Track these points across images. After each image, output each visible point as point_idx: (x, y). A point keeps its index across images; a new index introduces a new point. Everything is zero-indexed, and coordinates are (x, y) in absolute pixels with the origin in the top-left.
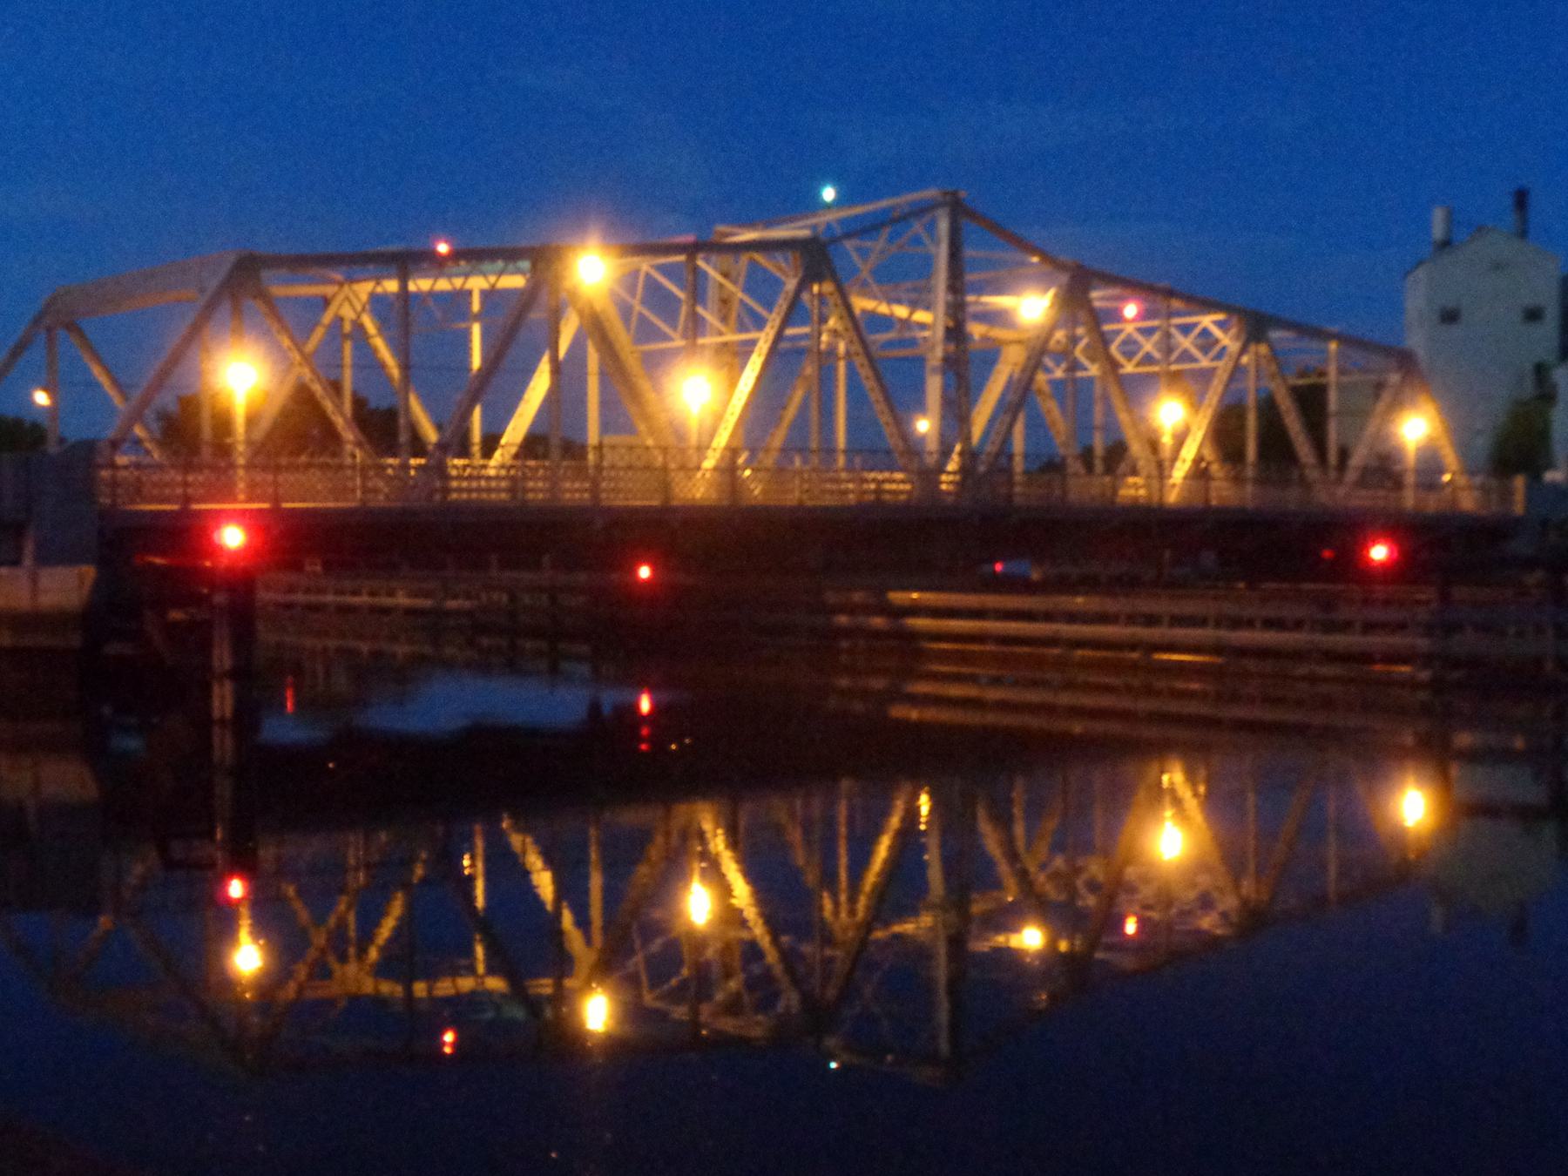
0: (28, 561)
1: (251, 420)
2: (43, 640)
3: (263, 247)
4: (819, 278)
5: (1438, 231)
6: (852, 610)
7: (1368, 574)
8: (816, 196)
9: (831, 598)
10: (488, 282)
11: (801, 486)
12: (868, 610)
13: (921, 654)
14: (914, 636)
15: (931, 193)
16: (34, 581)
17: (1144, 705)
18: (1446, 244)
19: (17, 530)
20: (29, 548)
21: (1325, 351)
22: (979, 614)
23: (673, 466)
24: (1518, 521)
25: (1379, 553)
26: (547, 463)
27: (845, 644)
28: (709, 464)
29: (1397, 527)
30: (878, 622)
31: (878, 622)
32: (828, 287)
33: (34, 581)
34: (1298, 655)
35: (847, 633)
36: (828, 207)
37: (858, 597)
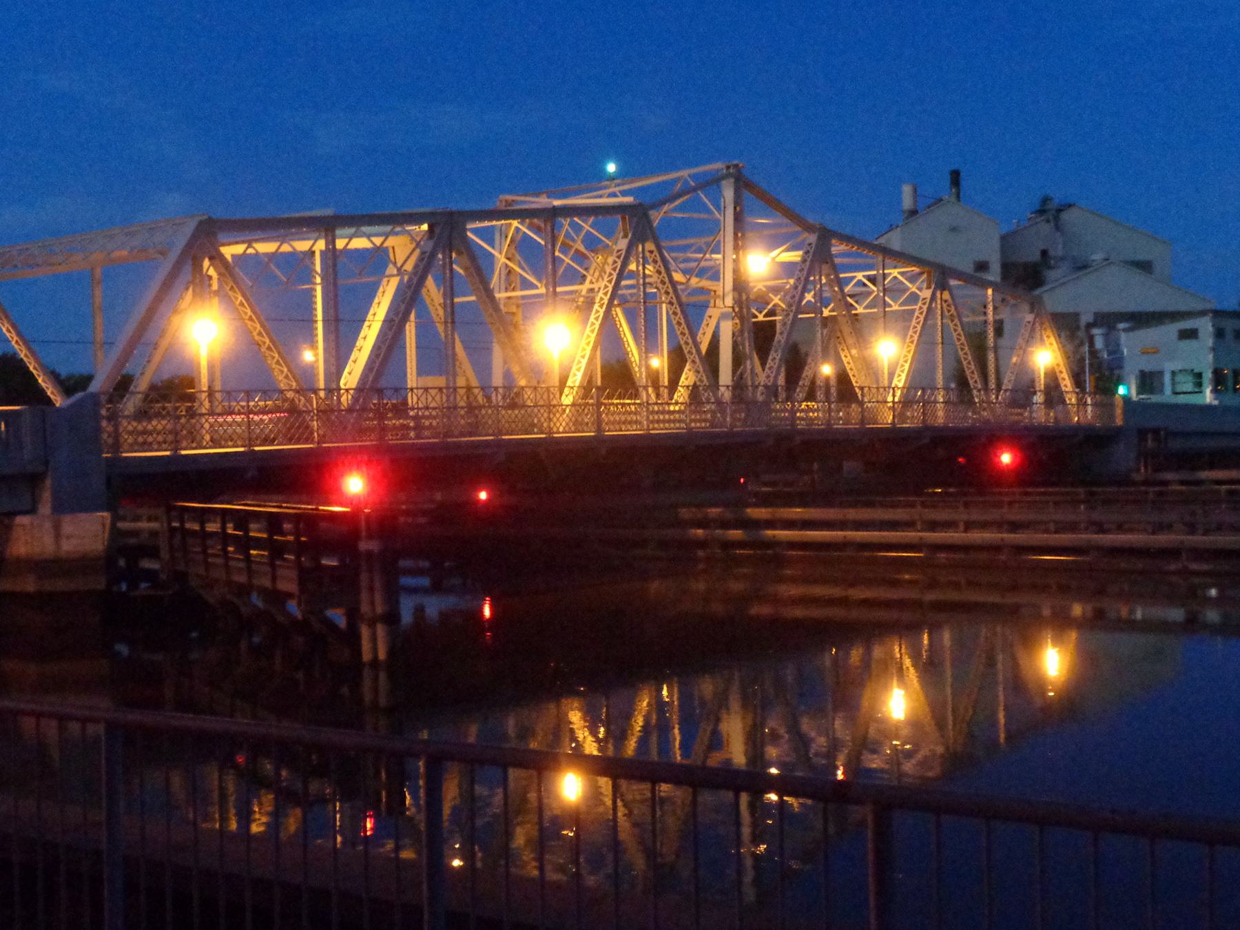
0: (45, 509)
1: (211, 367)
2: (61, 585)
3: (219, 213)
4: (643, 241)
5: (907, 202)
6: (704, 523)
7: (999, 477)
8: (603, 171)
9: (685, 513)
10: (254, 248)
11: (648, 417)
12: (726, 525)
13: (780, 561)
14: (773, 544)
15: (718, 165)
16: (57, 528)
17: (930, 596)
18: (913, 213)
19: (34, 480)
20: (47, 495)
21: (986, 296)
22: (842, 525)
23: (866, 400)
24: (1119, 431)
25: (1006, 458)
26: (638, 401)
27: (700, 553)
28: (567, 400)
29: (1019, 436)
30: (736, 534)
31: (736, 534)
32: (650, 246)
33: (57, 528)
34: (1172, 553)
35: (702, 544)
36: (612, 178)
37: (714, 511)
